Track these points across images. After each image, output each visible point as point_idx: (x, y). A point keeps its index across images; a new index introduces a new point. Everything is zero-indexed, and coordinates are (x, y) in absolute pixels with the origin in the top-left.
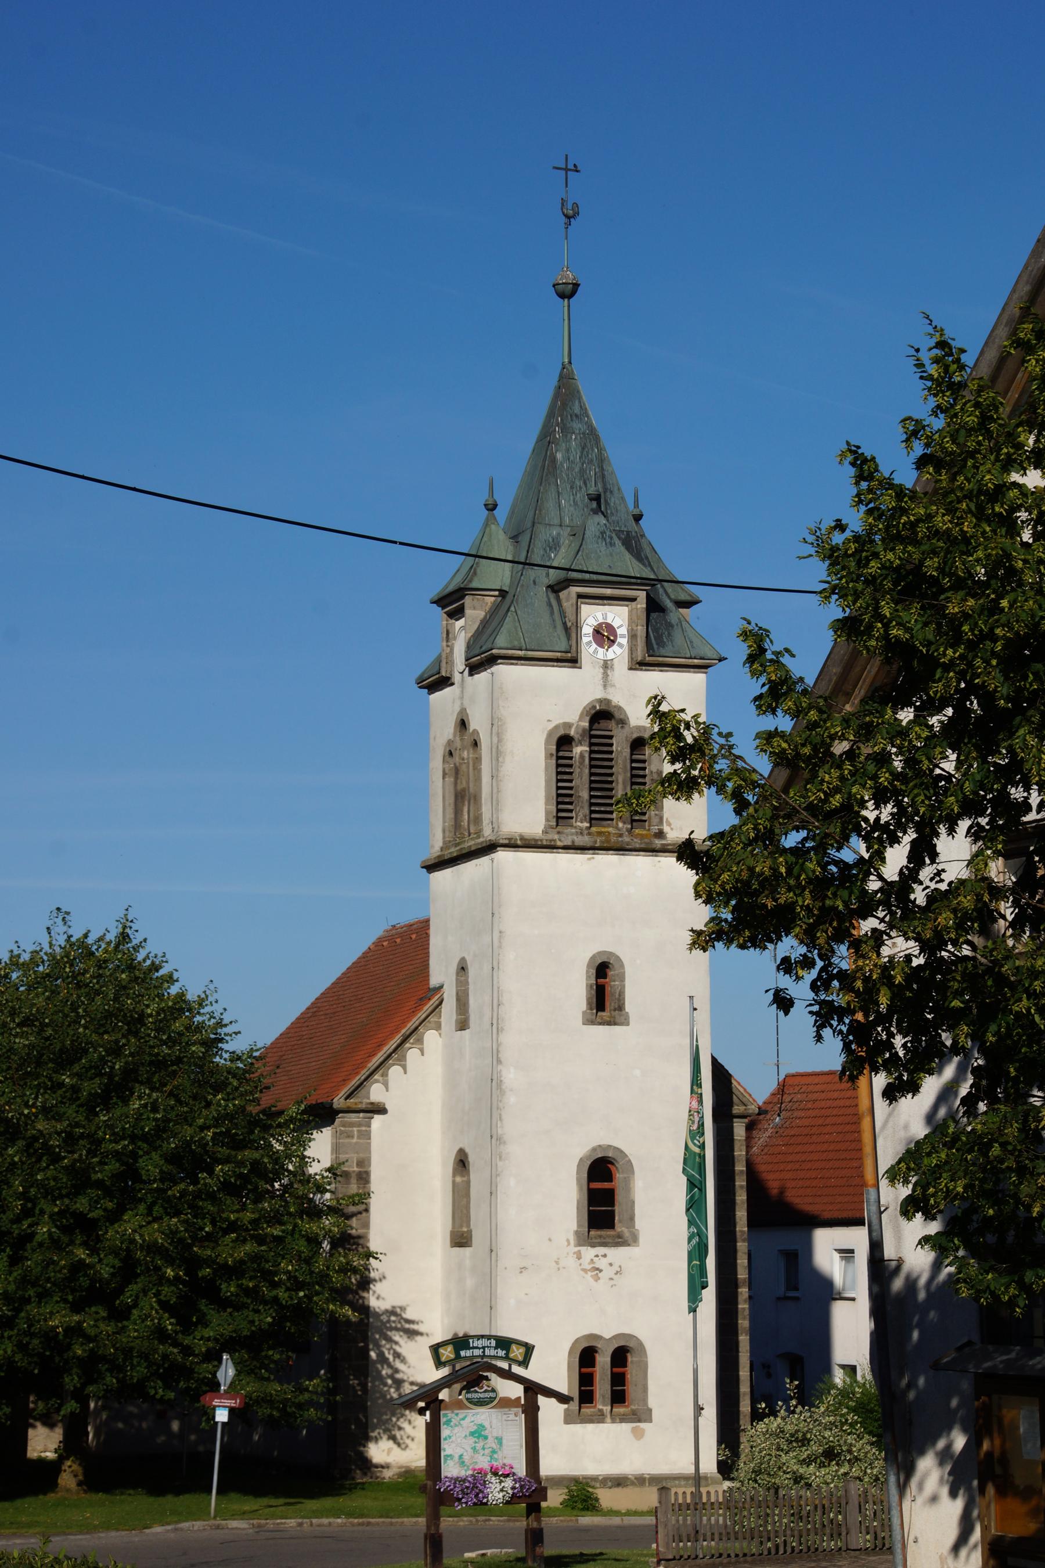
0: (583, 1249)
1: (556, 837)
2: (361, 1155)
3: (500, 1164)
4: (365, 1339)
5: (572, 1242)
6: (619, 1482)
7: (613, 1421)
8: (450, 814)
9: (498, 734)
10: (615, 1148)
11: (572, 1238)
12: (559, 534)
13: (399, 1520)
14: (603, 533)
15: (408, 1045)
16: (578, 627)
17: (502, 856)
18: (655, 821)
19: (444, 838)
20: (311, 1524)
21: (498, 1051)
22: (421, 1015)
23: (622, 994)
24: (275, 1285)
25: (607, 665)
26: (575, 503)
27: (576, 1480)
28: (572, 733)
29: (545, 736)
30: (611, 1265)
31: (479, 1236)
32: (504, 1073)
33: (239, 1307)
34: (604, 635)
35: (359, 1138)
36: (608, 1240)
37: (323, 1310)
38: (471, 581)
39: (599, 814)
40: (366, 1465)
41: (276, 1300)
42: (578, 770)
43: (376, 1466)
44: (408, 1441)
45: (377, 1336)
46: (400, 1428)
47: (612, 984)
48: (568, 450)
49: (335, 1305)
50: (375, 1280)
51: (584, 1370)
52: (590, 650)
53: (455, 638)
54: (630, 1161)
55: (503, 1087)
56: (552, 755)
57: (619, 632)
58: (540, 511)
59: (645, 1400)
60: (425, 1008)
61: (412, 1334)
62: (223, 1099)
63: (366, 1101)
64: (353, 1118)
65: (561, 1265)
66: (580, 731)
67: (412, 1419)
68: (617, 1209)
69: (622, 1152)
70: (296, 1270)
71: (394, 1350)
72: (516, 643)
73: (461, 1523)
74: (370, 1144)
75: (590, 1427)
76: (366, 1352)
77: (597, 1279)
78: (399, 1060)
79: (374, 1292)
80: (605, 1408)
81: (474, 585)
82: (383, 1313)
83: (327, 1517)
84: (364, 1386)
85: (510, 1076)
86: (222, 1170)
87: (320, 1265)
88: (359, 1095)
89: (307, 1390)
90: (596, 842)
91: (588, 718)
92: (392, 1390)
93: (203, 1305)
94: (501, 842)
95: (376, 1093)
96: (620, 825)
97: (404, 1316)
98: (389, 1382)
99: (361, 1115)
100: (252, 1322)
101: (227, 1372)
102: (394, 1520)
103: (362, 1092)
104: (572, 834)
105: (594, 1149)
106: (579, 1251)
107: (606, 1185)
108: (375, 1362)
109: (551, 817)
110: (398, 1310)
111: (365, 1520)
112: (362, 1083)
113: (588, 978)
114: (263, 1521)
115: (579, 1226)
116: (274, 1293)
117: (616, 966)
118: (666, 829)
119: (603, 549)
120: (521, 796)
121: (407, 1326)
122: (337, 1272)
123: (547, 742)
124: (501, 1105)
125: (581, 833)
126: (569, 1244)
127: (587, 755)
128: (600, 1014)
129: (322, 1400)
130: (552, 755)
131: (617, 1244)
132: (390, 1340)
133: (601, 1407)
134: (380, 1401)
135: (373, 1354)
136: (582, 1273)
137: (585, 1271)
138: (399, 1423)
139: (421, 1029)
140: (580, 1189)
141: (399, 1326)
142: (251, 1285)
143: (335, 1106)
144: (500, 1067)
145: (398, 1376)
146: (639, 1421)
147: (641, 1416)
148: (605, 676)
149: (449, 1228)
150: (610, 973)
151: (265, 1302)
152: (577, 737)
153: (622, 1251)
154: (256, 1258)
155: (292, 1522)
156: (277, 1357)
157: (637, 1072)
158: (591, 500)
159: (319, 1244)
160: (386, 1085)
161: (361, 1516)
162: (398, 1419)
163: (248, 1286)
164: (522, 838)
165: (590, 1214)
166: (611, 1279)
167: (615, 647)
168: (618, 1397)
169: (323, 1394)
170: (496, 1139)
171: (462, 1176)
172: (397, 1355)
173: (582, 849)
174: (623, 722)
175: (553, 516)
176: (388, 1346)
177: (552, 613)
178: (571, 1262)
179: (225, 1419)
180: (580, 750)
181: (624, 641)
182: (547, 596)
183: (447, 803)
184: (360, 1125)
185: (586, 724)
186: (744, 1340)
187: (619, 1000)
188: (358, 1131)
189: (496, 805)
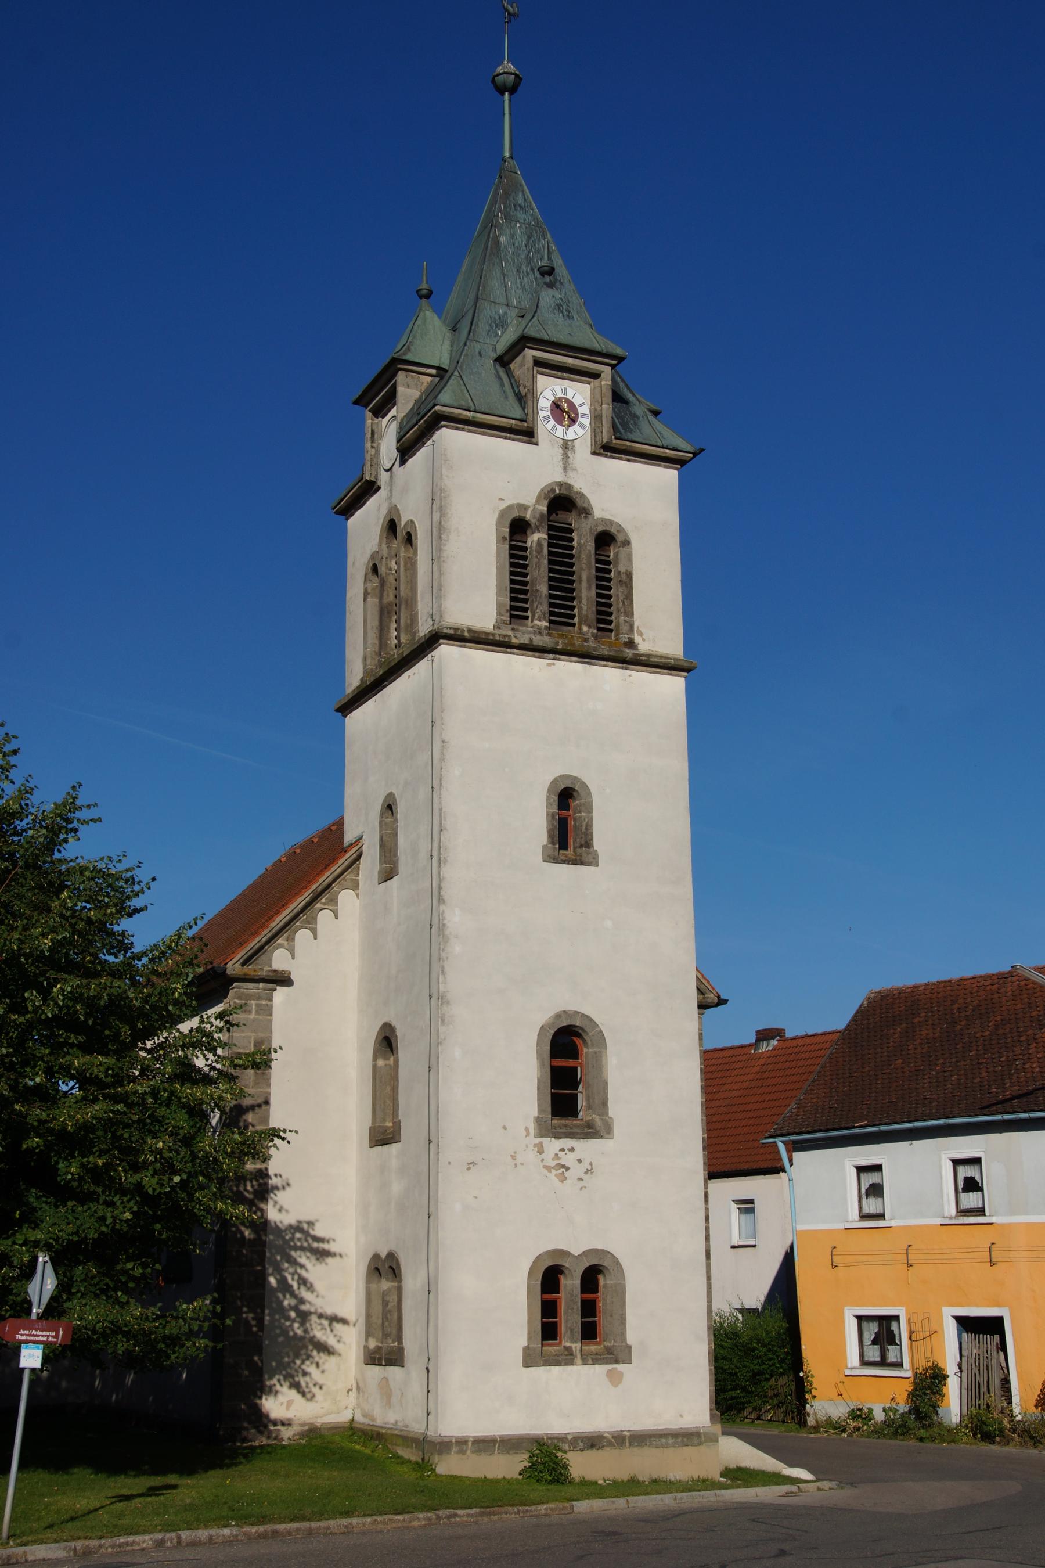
0: (546, 1141)
1: (510, 633)
2: (261, 1035)
3: (442, 1029)
4: (262, 1259)
5: (532, 1132)
6: (592, 1442)
7: (585, 1363)
9: (441, 508)
10: (583, 1015)
11: (532, 1126)
12: (506, 313)
13: (323, 1524)
14: (559, 306)
15: (318, 905)
16: (535, 400)
17: (446, 651)
18: (624, 628)
19: (365, 666)
21: (440, 888)
22: (336, 869)
23: (589, 827)
24: (136, 1168)
25: (567, 446)
26: (523, 287)
28: (528, 516)
29: (496, 516)
30: (580, 1161)
32: (447, 915)
33: (85, 1198)
34: (563, 411)
35: (257, 1013)
36: (575, 1130)
37: (208, 1210)
38: (405, 354)
39: (561, 614)
40: (261, 1421)
41: (139, 1186)
42: (535, 560)
43: (275, 1423)
44: (315, 1390)
45: (278, 1258)
46: (305, 1374)
48: (512, 236)
49: (226, 1204)
50: (277, 1188)
51: (548, 1297)
52: (546, 425)
53: (381, 437)
54: (601, 1031)
55: (447, 932)
56: (504, 538)
57: (580, 410)
58: (484, 287)
59: (623, 1335)
60: (341, 862)
61: (322, 1255)
62: (70, 897)
63: (266, 968)
64: (250, 988)
65: (519, 1159)
66: (537, 516)
67: (321, 1362)
69: (591, 1020)
70: (170, 1150)
71: (299, 1275)
72: (463, 403)
73: (416, 1523)
74: (271, 1021)
75: (556, 1370)
76: (263, 1277)
77: (563, 1179)
78: (309, 923)
79: (276, 1202)
80: (573, 1346)
81: (409, 357)
82: (286, 1229)
83: (206, 1527)
84: (260, 1321)
85: (455, 918)
86: (62, 990)
87: (205, 1145)
88: (260, 961)
90: (557, 643)
91: (546, 502)
92: (296, 1325)
93: (33, 1197)
94: (445, 631)
95: (279, 960)
96: (585, 628)
97: (312, 1232)
98: (293, 1314)
99: (261, 985)
100: (103, 1219)
101: (44, 1284)
102: (314, 1525)
103: (263, 958)
104: (530, 633)
105: (558, 1016)
106: (541, 1143)
107: (570, 1063)
108: (274, 1290)
109: (503, 611)
110: (305, 1226)
112: (262, 948)
113: (549, 805)
114: (94, 1543)
116: (137, 1177)
117: (582, 793)
118: (637, 639)
119: (561, 319)
120: (470, 585)
121: (315, 1245)
123: (499, 523)
124: (443, 955)
125: (540, 633)
126: (528, 1134)
127: (545, 544)
128: (562, 852)
130: (504, 538)
131: (587, 1136)
132: (294, 1263)
133: (568, 1344)
134: (281, 1339)
135: (272, 1280)
136: (545, 1171)
137: (547, 1168)
138: (304, 1367)
139: (335, 887)
140: (542, 1064)
141: (305, 1244)
142: (100, 1162)
143: (229, 972)
144: (442, 907)
145: (303, 1307)
146: (617, 1362)
147: (616, 1355)
148: (565, 458)
149: (368, 1123)
150: (573, 804)
151: (123, 1192)
152: (533, 522)
153: (593, 1143)
154: (110, 1124)
156: (138, 1272)
157: (609, 923)
158: (542, 274)
159: (205, 1117)
160: (292, 952)
161: (263, 1519)
162: (303, 1363)
163: (96, 1165)
164: (470, 630)
165: (554, 1097)
166: (581, 1179)
167: (576, 427)
168: (589, 1332)
170: (436, 998)
171: (387, 1059)
172: (303, 1282)
174: (586, 512)
175: (498, 294)
176: (291, 1270)
177: (502, 385)
178: (532, 1155)
179: (37, 1364)
180: (537, 538)
181: (586, 422)
182: (495, 369)
183: (369, 627)
184: (259, 998)
185: (544, 508)
187: (586, 835)
188: (257, 1005)
189: (437, 590)
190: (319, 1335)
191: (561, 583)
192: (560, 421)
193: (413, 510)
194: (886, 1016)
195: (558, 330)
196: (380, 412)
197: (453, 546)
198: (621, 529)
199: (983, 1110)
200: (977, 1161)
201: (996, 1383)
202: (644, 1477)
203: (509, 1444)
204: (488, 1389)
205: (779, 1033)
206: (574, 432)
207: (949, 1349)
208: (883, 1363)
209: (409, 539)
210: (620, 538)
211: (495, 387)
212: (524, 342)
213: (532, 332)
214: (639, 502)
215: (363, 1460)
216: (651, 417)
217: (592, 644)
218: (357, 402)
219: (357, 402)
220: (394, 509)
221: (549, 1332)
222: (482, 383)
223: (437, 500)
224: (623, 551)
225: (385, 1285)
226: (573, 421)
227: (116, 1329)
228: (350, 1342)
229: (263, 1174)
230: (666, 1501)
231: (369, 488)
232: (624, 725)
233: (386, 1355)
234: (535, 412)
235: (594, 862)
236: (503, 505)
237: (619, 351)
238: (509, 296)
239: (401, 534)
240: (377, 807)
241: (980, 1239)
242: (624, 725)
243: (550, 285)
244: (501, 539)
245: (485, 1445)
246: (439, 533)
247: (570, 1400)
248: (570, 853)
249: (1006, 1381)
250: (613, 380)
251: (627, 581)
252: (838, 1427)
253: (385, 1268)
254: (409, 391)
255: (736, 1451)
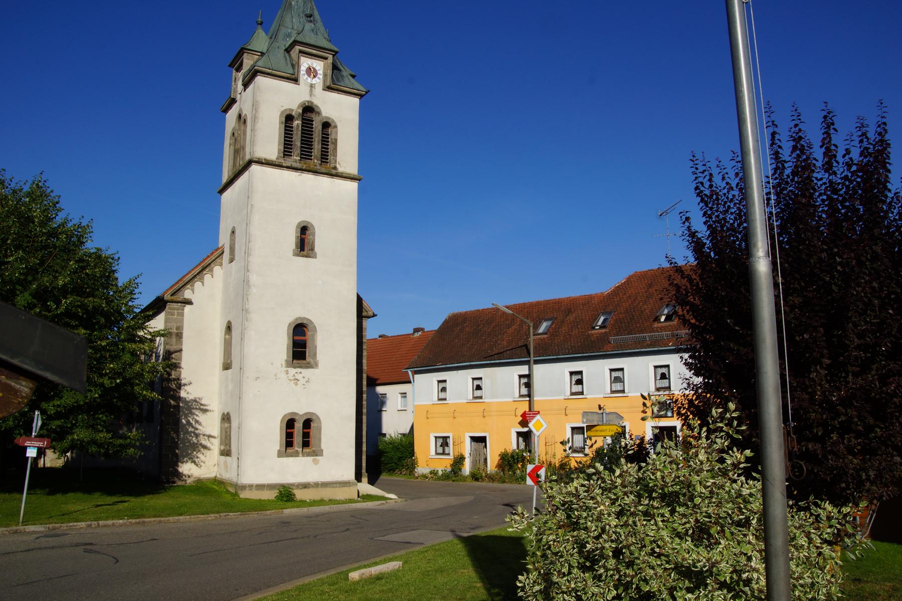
6: (306, 486)
8: (232, 161)
11: (284, 363)
16: (299, 66)
18: (333, 161)
20: (98, 525)
23: (313, 242)
25: (312, 86)
27: (283, 486)
31: (235, 365)
34: (311, 72)
39: (306, 154)
40: (179, 475)
41: (102, 385)
47: (308, 237)
59: (320, 445)
64: (175, 305)
68: (307, 350)
77: (296, 384)
81: (249, 47)
85: (254, 278)
89: (129, 437)
95: (187, 294)
102: (162, 519)
103: (180, 294)
105: (297, 319)
107: (302, 338)
108: (185, 425)
111: (141, 520)
115: (288, 357)
118: (338, 166)
120: (267, 140)
122: (148, 372)
129: (138, 444)
131: (307, 367)
135: (184, 421)
139: (212, 265)
140: (289, 338)
147: (318, 453)
148: (311, 91)
150: (307, 233)
155: (83, 524)
156: (104, 418)
161: (139, 517)
168: (306, 444)
169: (138, 440)
170: (245, 311)
172: (197, 422)
173: (296, 169)
174: (319, 113)
178: (283, 375)
180: (297, 123)
181: (321, 77)
184: (178, 309)
186: (364, 417)
189: (253, 143)
190: (204, 442)
191: (307, 143)
192: (309, 76)
193: (247, 111)
194: (454, 323)
195: (311, 39)
196: (239, 69)
197: (260, 125)
198: (333, 121)
199: (485, 358)
200: (481, 379)
201: (482, 460)
202: (326, 498)
203: (271, 487)
204: (261, 465)
205: (422, 329)
206: (315, 81)
207: (467, 448)
208: (443, 453)
209: (245, 122)
210: (333, 125)
211: (283, 61)
212: (295, 43)
213: (299, 39)
214: (342, 111)
215: (216, 493)
216: (351, 78)
217: (318, 167)
218: (230, 66)
219: (230, 66)
220: (241, 110)
221: (289, 444)
222: (278, 59)
223: (255, 106)
224: (334, 130)
225: (227, 425)
226: (315, 77)
227: (94, 442)
228: (215, 446)
229: (178, 379)
230: (335, 508)
231: (233, 101)
232: (331, 201)
233: (226, 453)
234: (299, 72)
235: (315, 257)
236: (283, 109)
237: (336, 49)
238: (293, 24)
239: (242, 120)
240: (230, 232)
241: (480, 408)
242: (331, 201)
243: (311, 21)
244: (281, 123)
245: (260, 487)
246: (255, 118)
247: (297, 470)
248: (305, 253)
249: (486, 459)
250: (333, 60)
251: (335, 142)
252: (425, 476)
253: (226, 418)
254: (248, 62)
255: (365, 487)
